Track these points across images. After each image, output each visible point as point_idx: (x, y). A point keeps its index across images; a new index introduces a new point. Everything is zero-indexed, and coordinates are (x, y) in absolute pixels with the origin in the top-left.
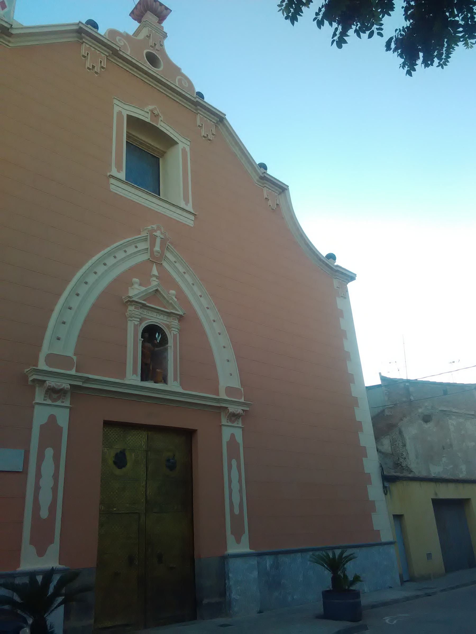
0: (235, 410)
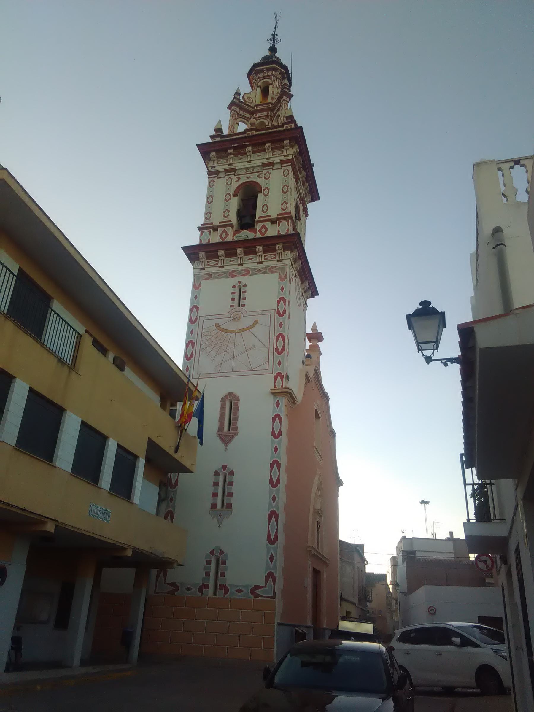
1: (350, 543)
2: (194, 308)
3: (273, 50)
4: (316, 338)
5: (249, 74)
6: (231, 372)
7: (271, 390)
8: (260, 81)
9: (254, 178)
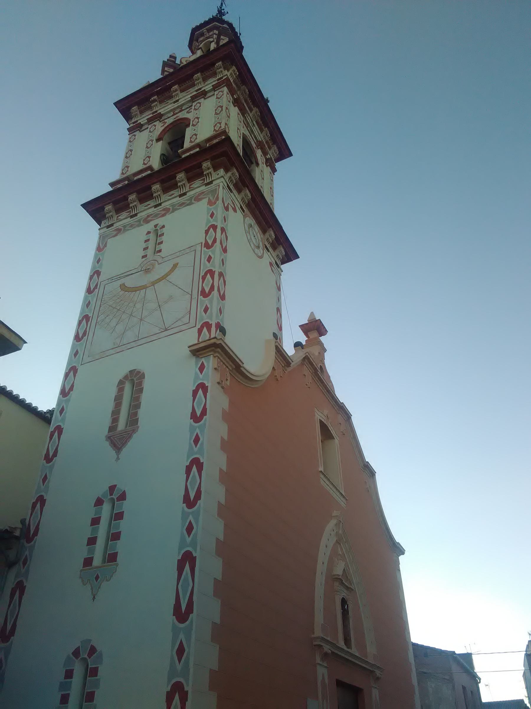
1: (443, 649)
2: (96, 273)
4: (314, 330)
7: (188, 347)
9: (183, 115)
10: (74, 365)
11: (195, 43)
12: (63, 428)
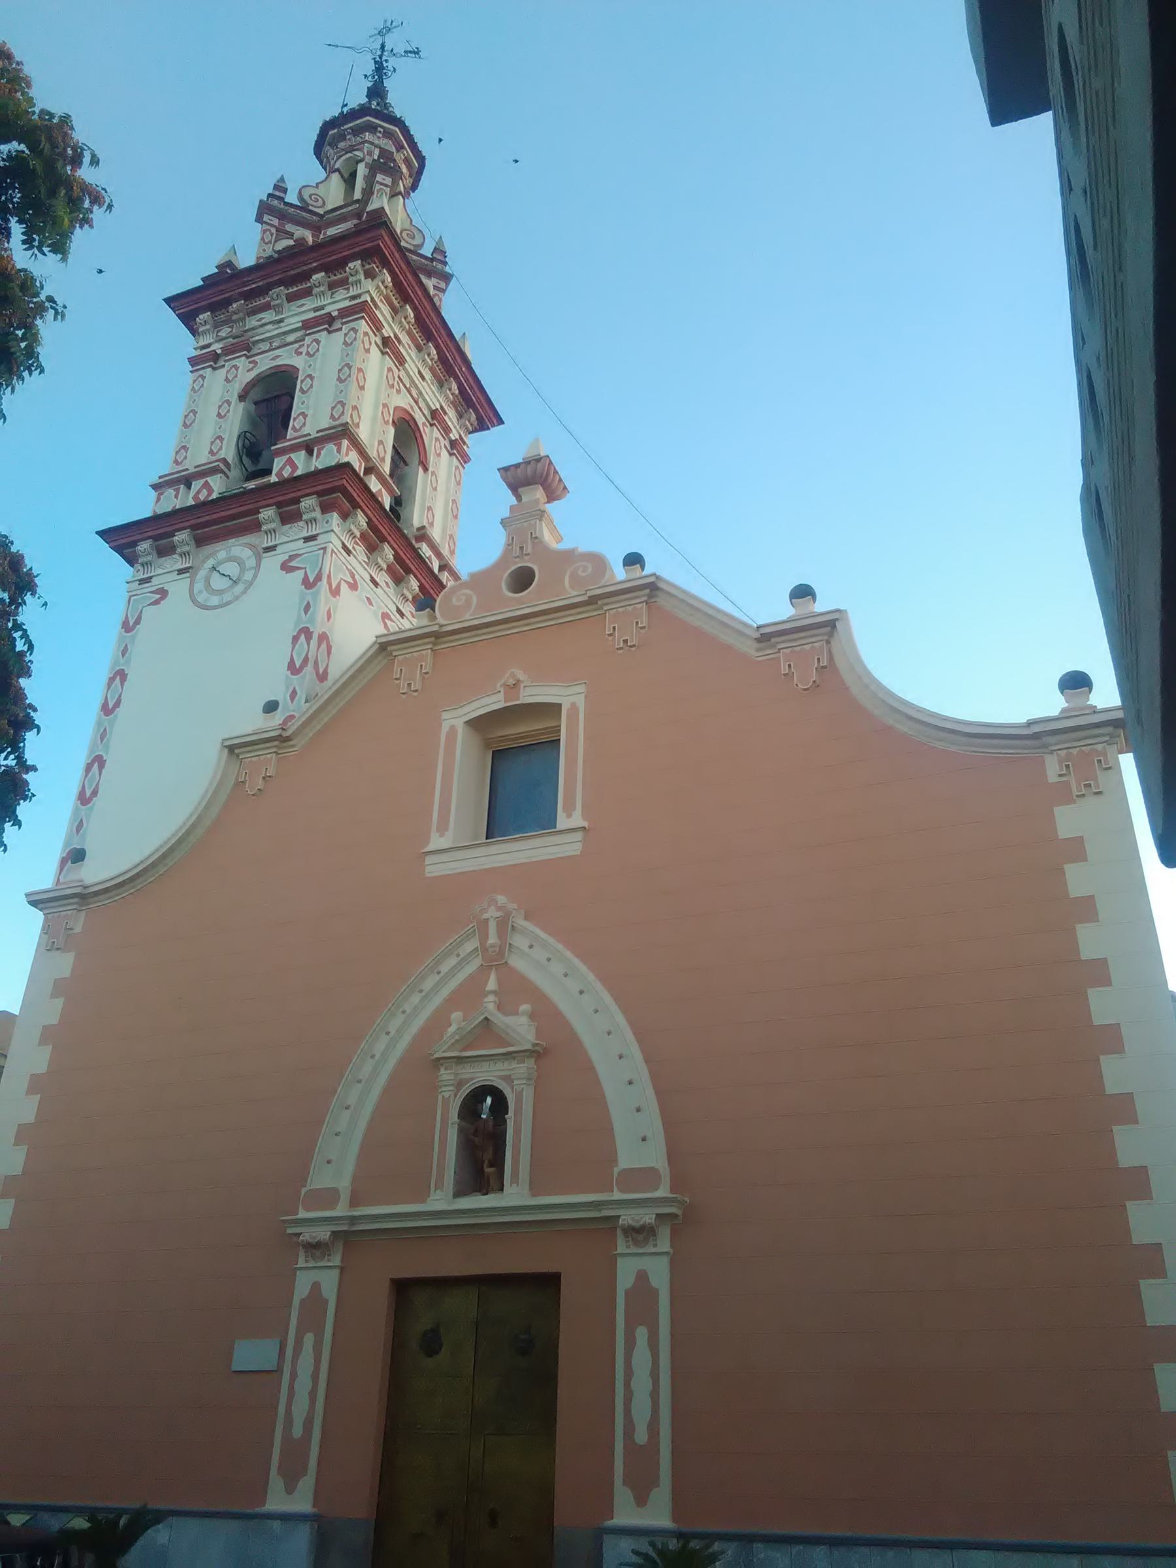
0: (633, 1219)
3: (377, 91)
5: (318, 150)
6: (784, 648)
8: (337, 160)
9: (286, 358)
10: (101, 753)
11: (328, 150)
12: (106, 760)
